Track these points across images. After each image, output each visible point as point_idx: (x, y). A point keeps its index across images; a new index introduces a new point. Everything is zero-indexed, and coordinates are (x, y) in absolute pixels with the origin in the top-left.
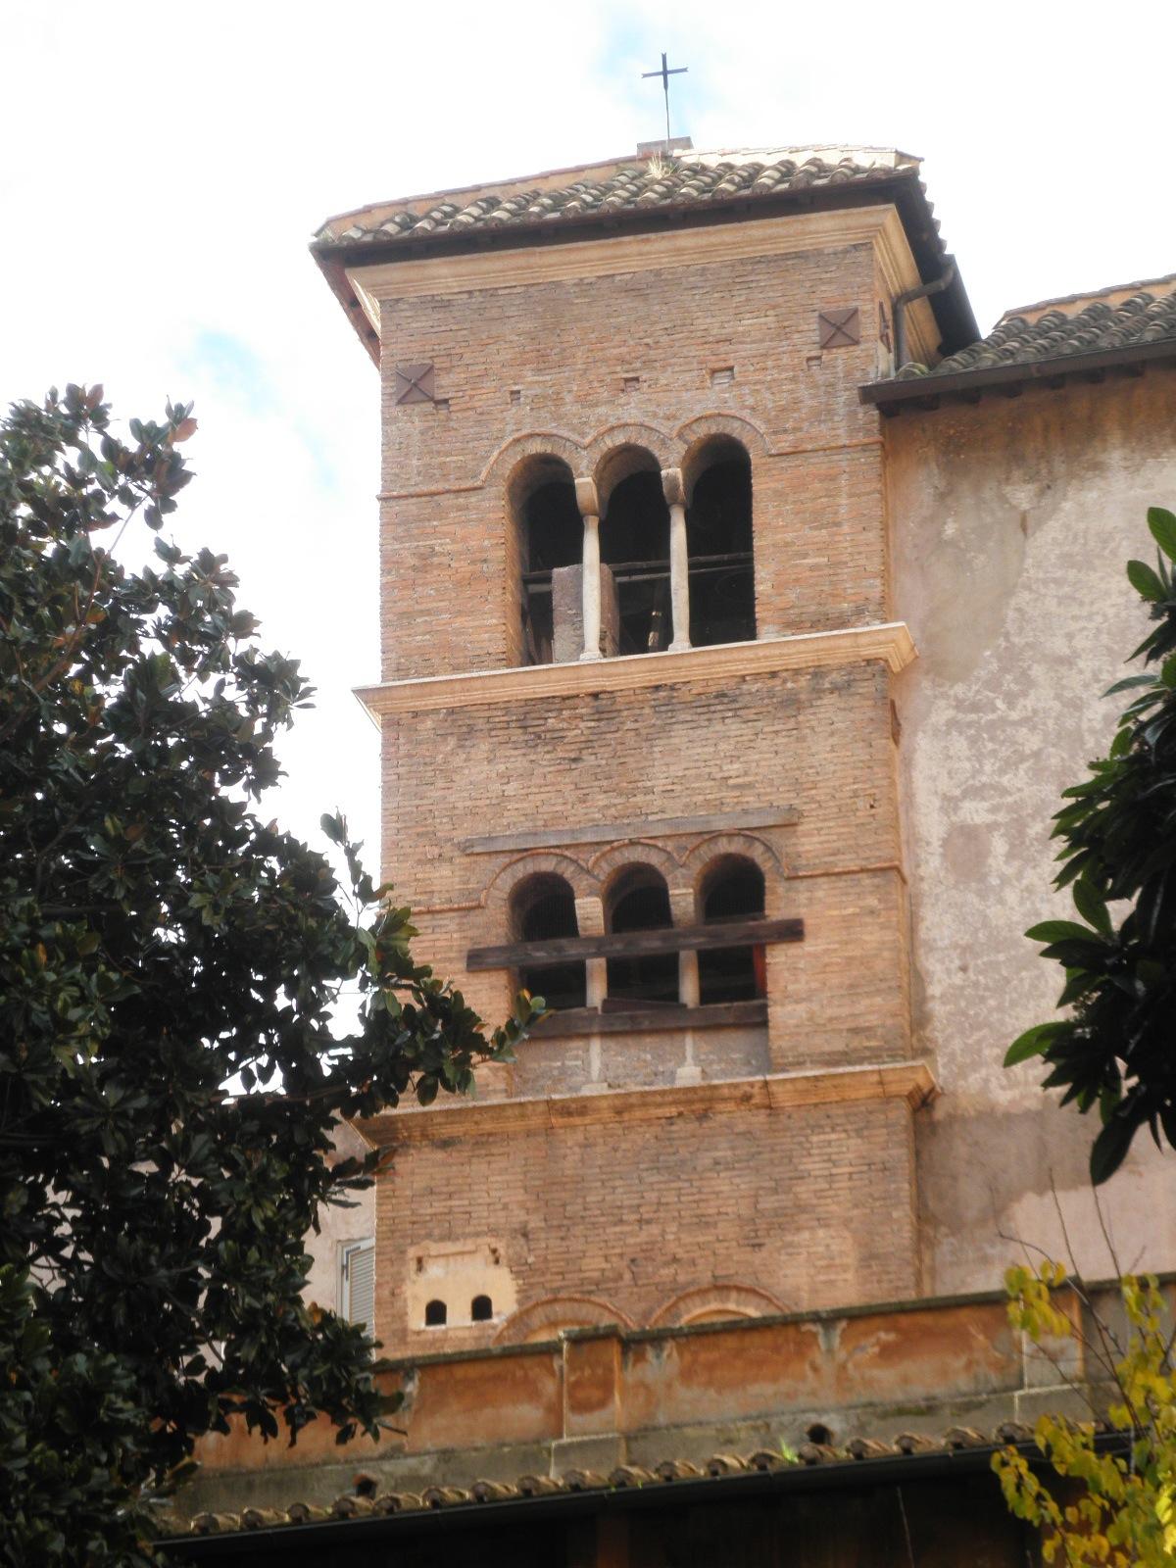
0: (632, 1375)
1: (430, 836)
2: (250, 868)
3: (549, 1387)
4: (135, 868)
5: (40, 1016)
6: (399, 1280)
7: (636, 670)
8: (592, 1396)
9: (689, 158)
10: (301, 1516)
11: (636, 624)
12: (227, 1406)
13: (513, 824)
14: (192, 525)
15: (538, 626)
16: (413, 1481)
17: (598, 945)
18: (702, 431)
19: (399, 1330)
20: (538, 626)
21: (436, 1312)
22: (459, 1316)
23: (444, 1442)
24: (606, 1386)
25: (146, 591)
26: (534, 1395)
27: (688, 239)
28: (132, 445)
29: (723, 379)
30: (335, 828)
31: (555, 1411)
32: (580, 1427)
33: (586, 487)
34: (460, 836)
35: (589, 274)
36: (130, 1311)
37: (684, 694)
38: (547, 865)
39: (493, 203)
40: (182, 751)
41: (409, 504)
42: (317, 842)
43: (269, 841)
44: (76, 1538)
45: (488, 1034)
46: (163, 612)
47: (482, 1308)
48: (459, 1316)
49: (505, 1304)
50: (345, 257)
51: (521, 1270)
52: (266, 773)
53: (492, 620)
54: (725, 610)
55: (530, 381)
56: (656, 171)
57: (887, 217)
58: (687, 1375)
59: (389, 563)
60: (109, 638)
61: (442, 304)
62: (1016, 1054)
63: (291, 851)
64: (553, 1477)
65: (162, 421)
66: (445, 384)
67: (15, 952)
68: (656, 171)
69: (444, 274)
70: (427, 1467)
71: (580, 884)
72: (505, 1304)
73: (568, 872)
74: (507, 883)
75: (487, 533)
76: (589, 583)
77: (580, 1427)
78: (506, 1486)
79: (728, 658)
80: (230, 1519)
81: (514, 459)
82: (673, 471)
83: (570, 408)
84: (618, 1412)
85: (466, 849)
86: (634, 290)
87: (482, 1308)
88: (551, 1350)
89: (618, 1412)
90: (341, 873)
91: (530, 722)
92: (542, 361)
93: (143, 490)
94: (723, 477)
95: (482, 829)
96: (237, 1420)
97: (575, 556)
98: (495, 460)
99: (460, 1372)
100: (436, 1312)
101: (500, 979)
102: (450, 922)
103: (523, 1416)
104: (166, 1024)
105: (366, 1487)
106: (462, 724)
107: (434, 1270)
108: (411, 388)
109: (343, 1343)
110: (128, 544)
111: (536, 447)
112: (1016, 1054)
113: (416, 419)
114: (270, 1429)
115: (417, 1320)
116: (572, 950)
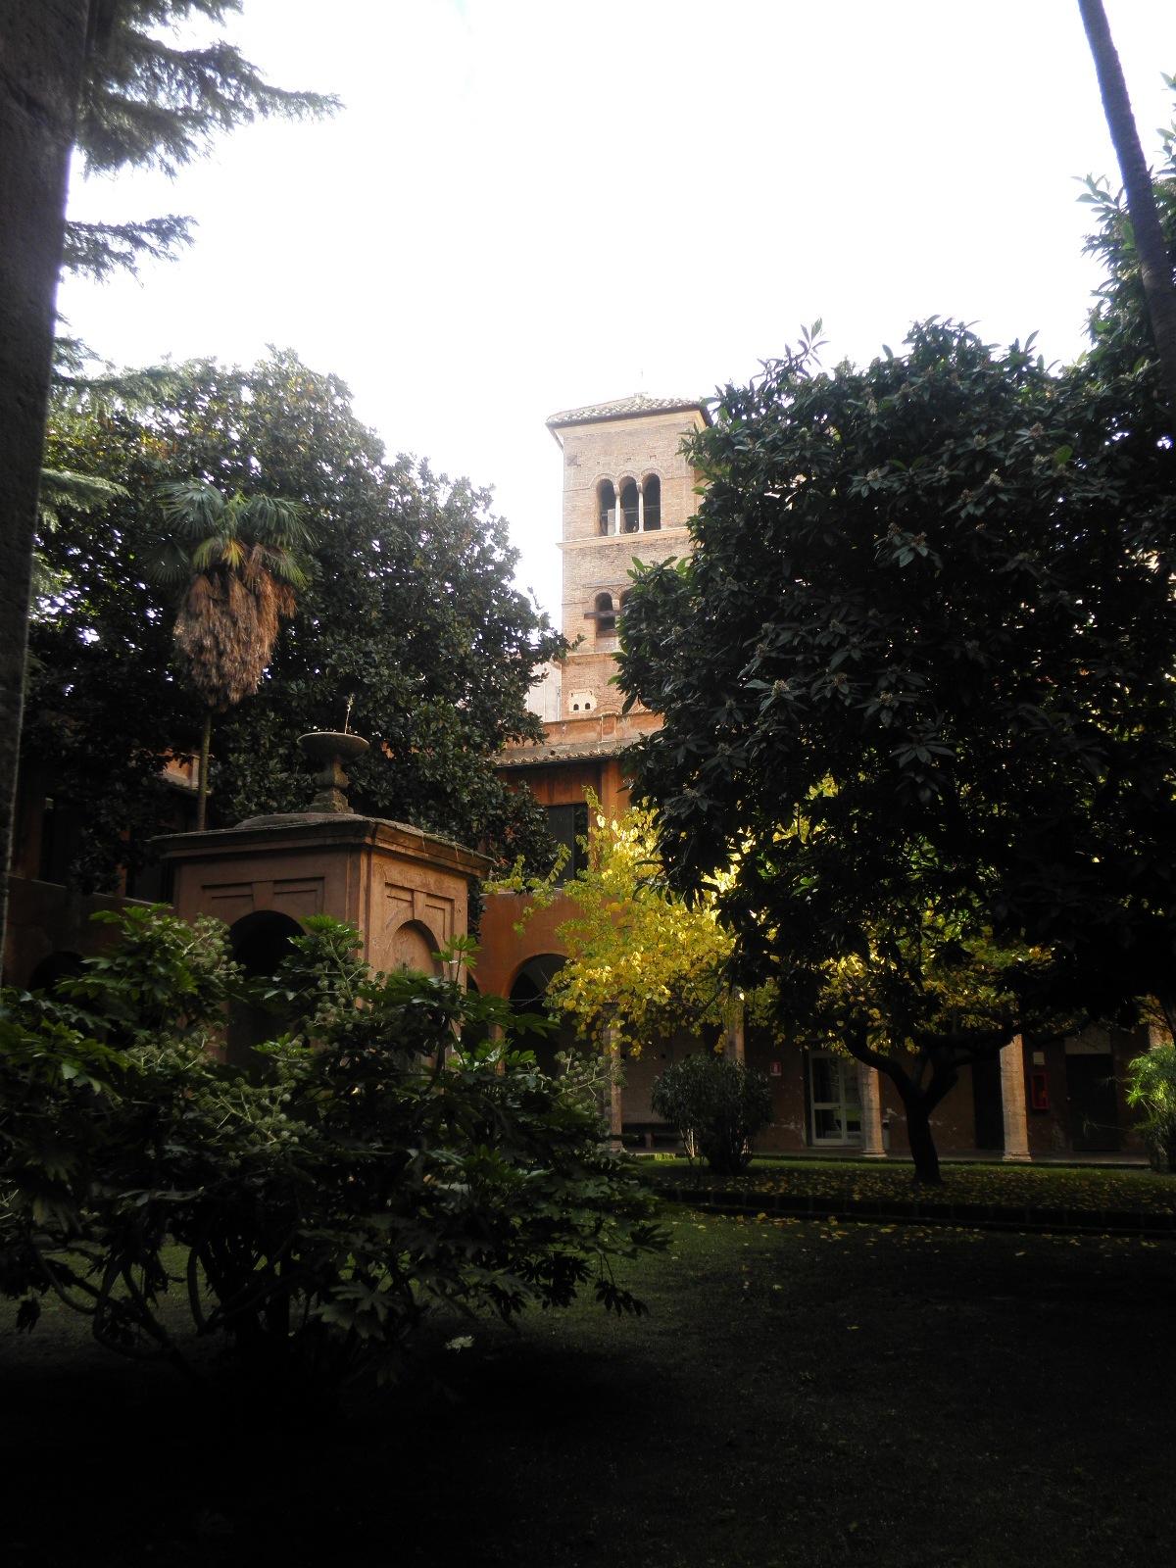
0: (619, 725)
1: (574, 583)
2: (510, 600)
3: (598, 728)
4: (480, 602)
5: (455, 641)
6: (567, 699)
7: (630, 537)
8: (609, 731)
9: (647, 397)
10: (536, 760)
11: (630, 525)
12: (509, 736)
13: (596, 580)
14: (494, 508)
15: (604, 525)
16: (564, 751)
17: (618, 612)
18: (647, 473)
19: (548, 716)
20: (604, 525)
21: (576, 707)
22: (582, 708)
23: (572, 741)
24: (612, 728)
25: (487, 526)
26: (594, 730)
27: (645, 420)
28: (479, 493)
29: (653, 459)
30: (531, 590)
31: (600, 734)
32: (606, 738)
33: (617, 488)
34: (583, 582)
35: (618, 430)
36: (483, 716)
37: (641, 544)
38: (605, 591)
39: (594, 411)
40: (749, 416)
41: (572, 492)
42: (526, 594)
43: (514, 594)
44: (464, 772)
45: (570, 644)
46: (492, 532)
47: (588, 706)
48: (582, 708)
49: (593, 706)
50: (554, 426)
51: (598, 697)
52: (513, 576)
53: (591, 524)
54: (653, 521)
55: (602, 459)
56: (638, 401)
57: (697, 414)
58: (633, 726)
59: (565, 509)
60: (478, 538)
61: (580, 439)
62: (610, 683)
63: (520, 596)
64: (598, 751)
65: (487, 487)
66: (580, 460)
67: (449, 625)
68: (638, 401)
69: (579, 430)
70: (568, 748)
71: (613, 596)
72: (593, 706)
73: (610, 593)
74: (594, 595)
75: (591, 501)
76: (617, 513)
77: (606, 738)
78: (586, 753)
79: (653, 534)
80: (518, 761)
81: (598, 480)
82: (639, 484)
83: (613, 466)
84: (615, 735)
85: (584, 586)
86: (630, 434)
87: (588, 706)
88: (599, 719)
89: (615, 735)
90: (532, 602)
91: (601, 552)
92: (606, 453)
93: (481, 503)
94: (653, 485)
95: (588, 581)
96: (511, 739)
97: (613, 507)
98: (593, 480)
99: (577, 724)
100: (576, 707)
101: (593, 621)
102: (580, 606)
103: (592, 735)
104: (495, 638)
105: (553, 753)
106: (583, 552)
107: (576, 696)
108: (572, 461)
109: (533, 720)
110: (481, 515)
111: (604, 477)
112: (610, 683)
113: (572, 470)
114: (518, 741)
115: (571, 709)
116: (611, 613)
